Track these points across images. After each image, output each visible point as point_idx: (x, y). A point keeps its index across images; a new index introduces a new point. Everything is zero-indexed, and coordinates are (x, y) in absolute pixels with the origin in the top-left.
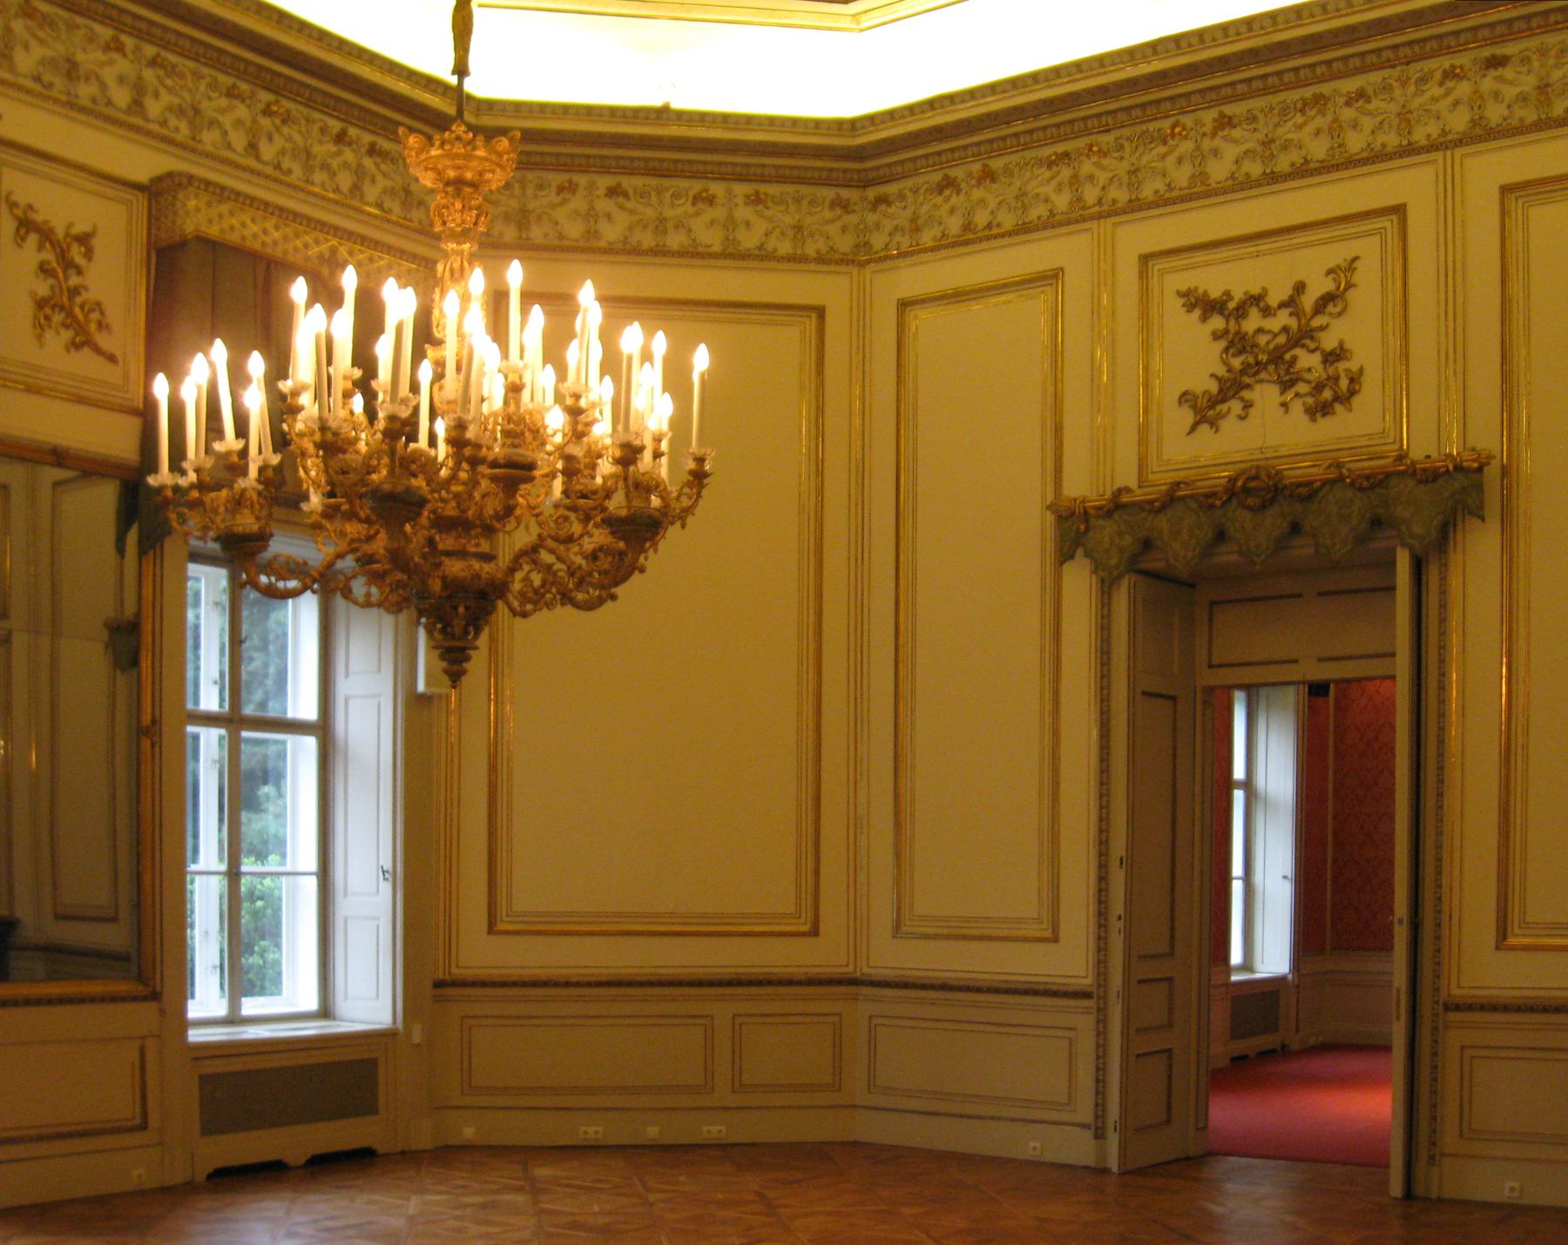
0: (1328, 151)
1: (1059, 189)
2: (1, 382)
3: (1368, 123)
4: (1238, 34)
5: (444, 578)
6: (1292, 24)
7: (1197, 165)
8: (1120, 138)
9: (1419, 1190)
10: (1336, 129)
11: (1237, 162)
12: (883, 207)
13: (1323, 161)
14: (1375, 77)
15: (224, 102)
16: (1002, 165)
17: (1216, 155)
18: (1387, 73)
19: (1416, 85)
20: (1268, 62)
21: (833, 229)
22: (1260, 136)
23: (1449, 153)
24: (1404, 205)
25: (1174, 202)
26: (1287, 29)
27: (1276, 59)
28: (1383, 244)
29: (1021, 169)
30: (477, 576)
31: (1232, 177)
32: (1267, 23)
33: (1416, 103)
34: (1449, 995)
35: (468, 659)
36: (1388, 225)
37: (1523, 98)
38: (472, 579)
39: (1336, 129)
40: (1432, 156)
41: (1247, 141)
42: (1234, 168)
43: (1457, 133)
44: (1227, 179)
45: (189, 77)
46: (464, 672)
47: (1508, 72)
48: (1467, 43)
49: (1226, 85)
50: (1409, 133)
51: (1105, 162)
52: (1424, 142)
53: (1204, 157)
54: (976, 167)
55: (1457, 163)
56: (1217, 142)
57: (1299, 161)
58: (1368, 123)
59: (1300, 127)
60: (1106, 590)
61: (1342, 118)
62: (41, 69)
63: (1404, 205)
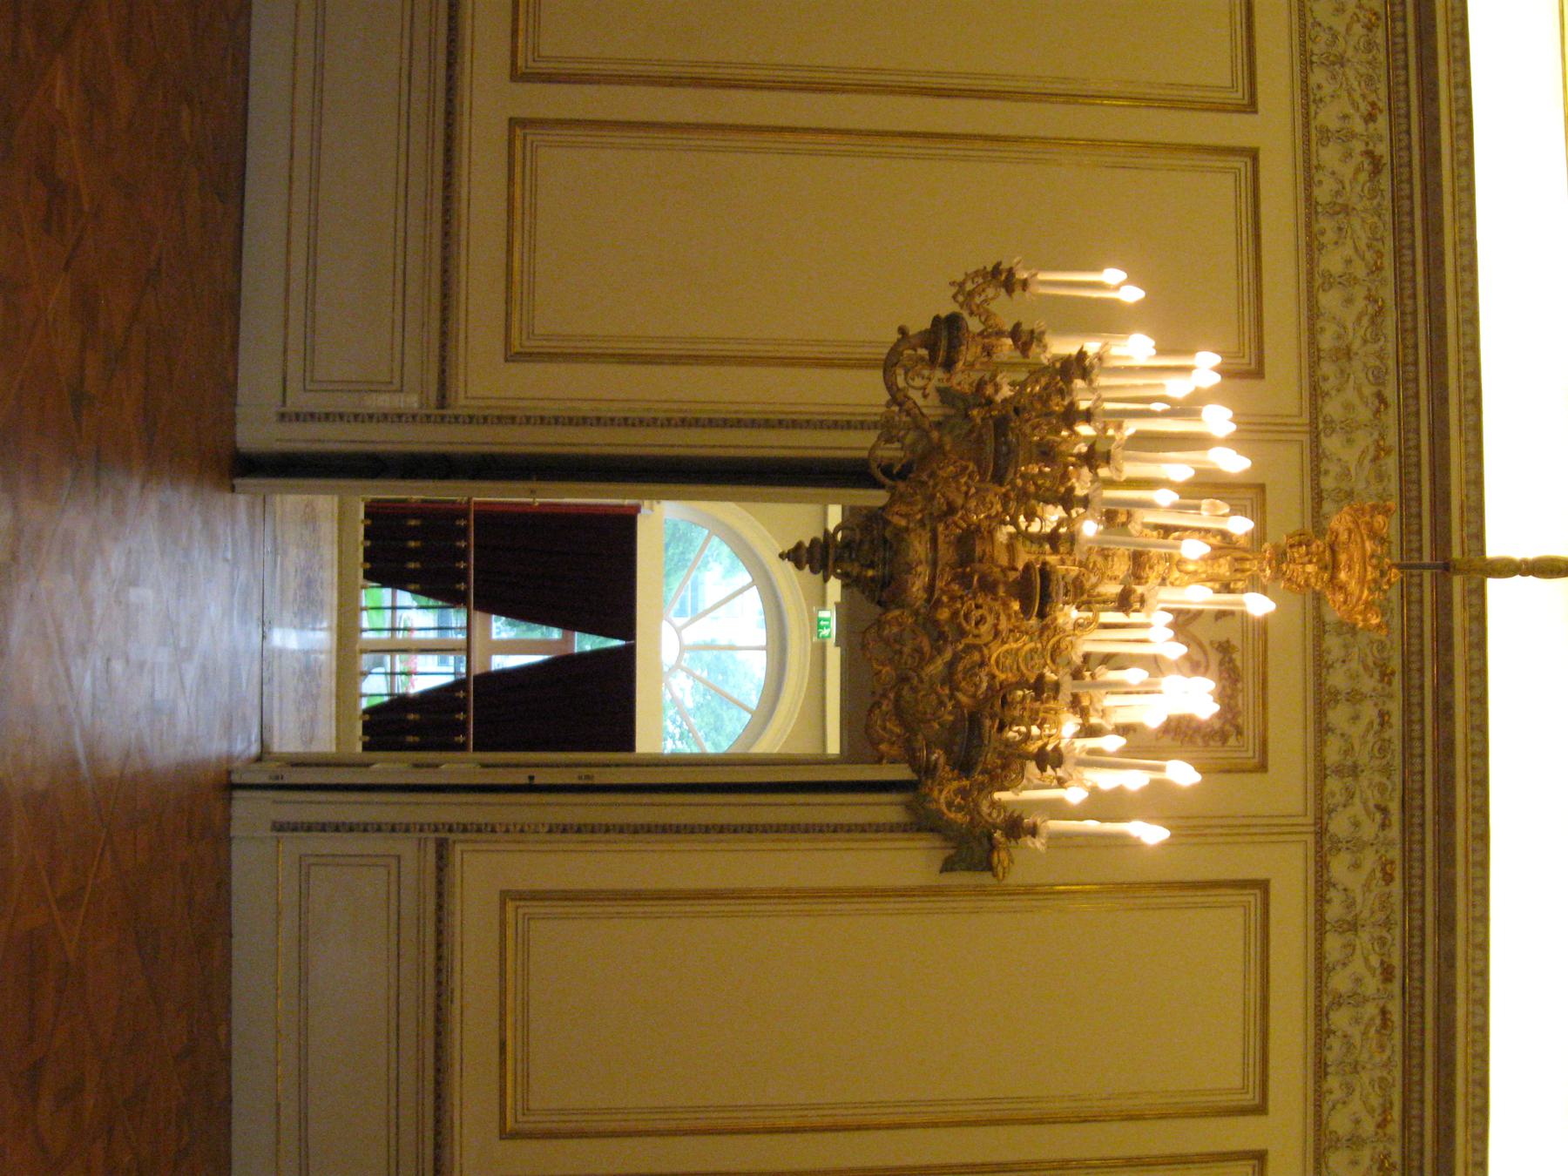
0: (1335, 687)
1: (1354, 677)
2: (1415, 1172)
3: (1347, 171)
4: (1474, 1041)
5: (907, 529)
6: (1462, 367)
7: (1343, 425)
8: (1378, 49)
9: (237, 794)
10: (1354, 697)
11: (1330, 28)
12: (1367, 166)
13: (1327, 1124)
14: (1394, 487)
15: (1375, 961)
16: (1377, 41)
17: (1337, 10)
18: (1388, 195)
19: (1380, 783)
20: (1423, 139)
21: (1357, 808)
22: (1350, 53)
23: (1307, 429)
24: (1256, 112)
25: (1318, 1106)
26: (1467, 862)
27: (1423, 149)
28: (1221, 88)
29: (1370, 63)
30: (910, 568)
31: (1318, 168)
32: (1479, 939)
33: (1350, 73)
34: (454, 842)
35: (814, 571)
36: (1252, 899)
37: (1350, 905)
38: (907, 563)
39: (1348, 280)
40: (1306, 414)
41: (1352, 189)
42: (1325, 25)
43: (1327, 824)
44: (1314, 18)
45: (1385, 1056)
46: (799, 565)
47: (1378, 887)
48: (1405, 389)
49: (1423, 870)
50: (1323, 63)
51: (1365, 321)
52: (1325, 1087)
53: (1347, 432)
54: (1382, 149)
55: (1296, 437)
56: (1357, 159)
57: (1326, 386)
58: (1339, 24)
59: (1359, 390)
60: (882, 415)
61: (1354, 141)
62: (1339, 1033)
63: (1256, 112)
